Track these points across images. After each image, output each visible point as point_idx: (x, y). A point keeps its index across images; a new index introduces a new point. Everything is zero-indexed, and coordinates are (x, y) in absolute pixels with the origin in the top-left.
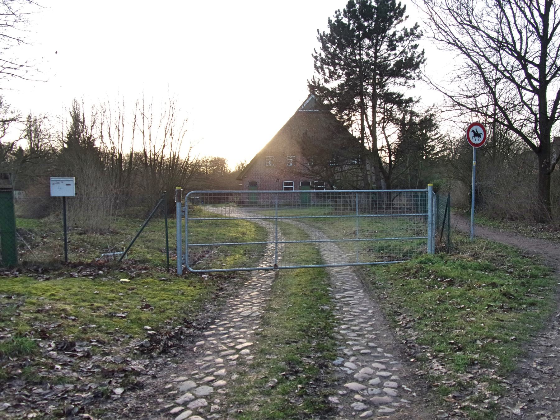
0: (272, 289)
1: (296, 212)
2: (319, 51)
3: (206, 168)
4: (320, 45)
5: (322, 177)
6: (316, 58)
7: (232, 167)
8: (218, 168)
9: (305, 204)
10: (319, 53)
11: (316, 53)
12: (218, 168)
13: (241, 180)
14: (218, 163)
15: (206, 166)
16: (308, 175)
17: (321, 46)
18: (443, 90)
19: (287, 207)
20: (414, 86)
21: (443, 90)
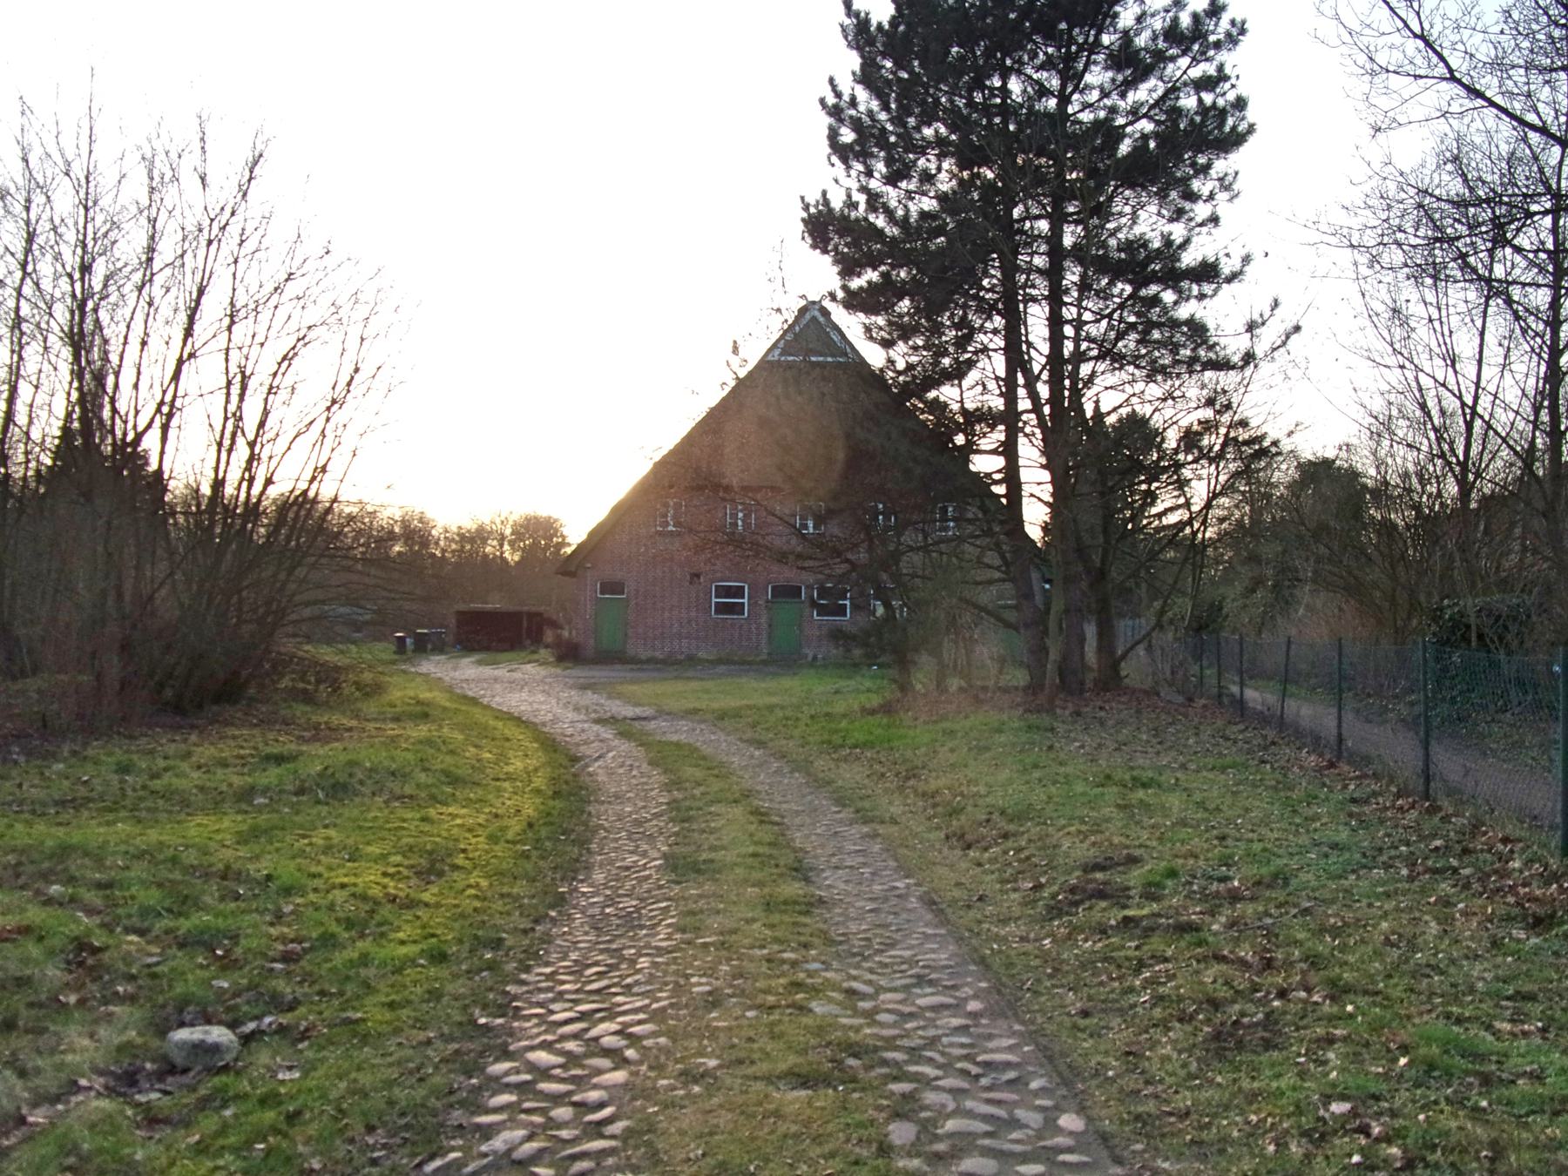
0: (305, 1075)
1: (754, 691)
2: (846, 85)
3: (501, 546)
4: (854, 61)
5: (854, 566)
6: (835, 112)
7: (575, 533)
8: (535, 544)
9: (784, 660)
10: (846, 98)
11: (838, 95)
12: (535, 544)
13: (572, 574)
14: (538, 532)
15: (502, 538)
16: (799, 556)
17: (857, 69)
18: (1317, 332)
19: (722, 669)
20: (1214, 220)
21: (1317, 332)
